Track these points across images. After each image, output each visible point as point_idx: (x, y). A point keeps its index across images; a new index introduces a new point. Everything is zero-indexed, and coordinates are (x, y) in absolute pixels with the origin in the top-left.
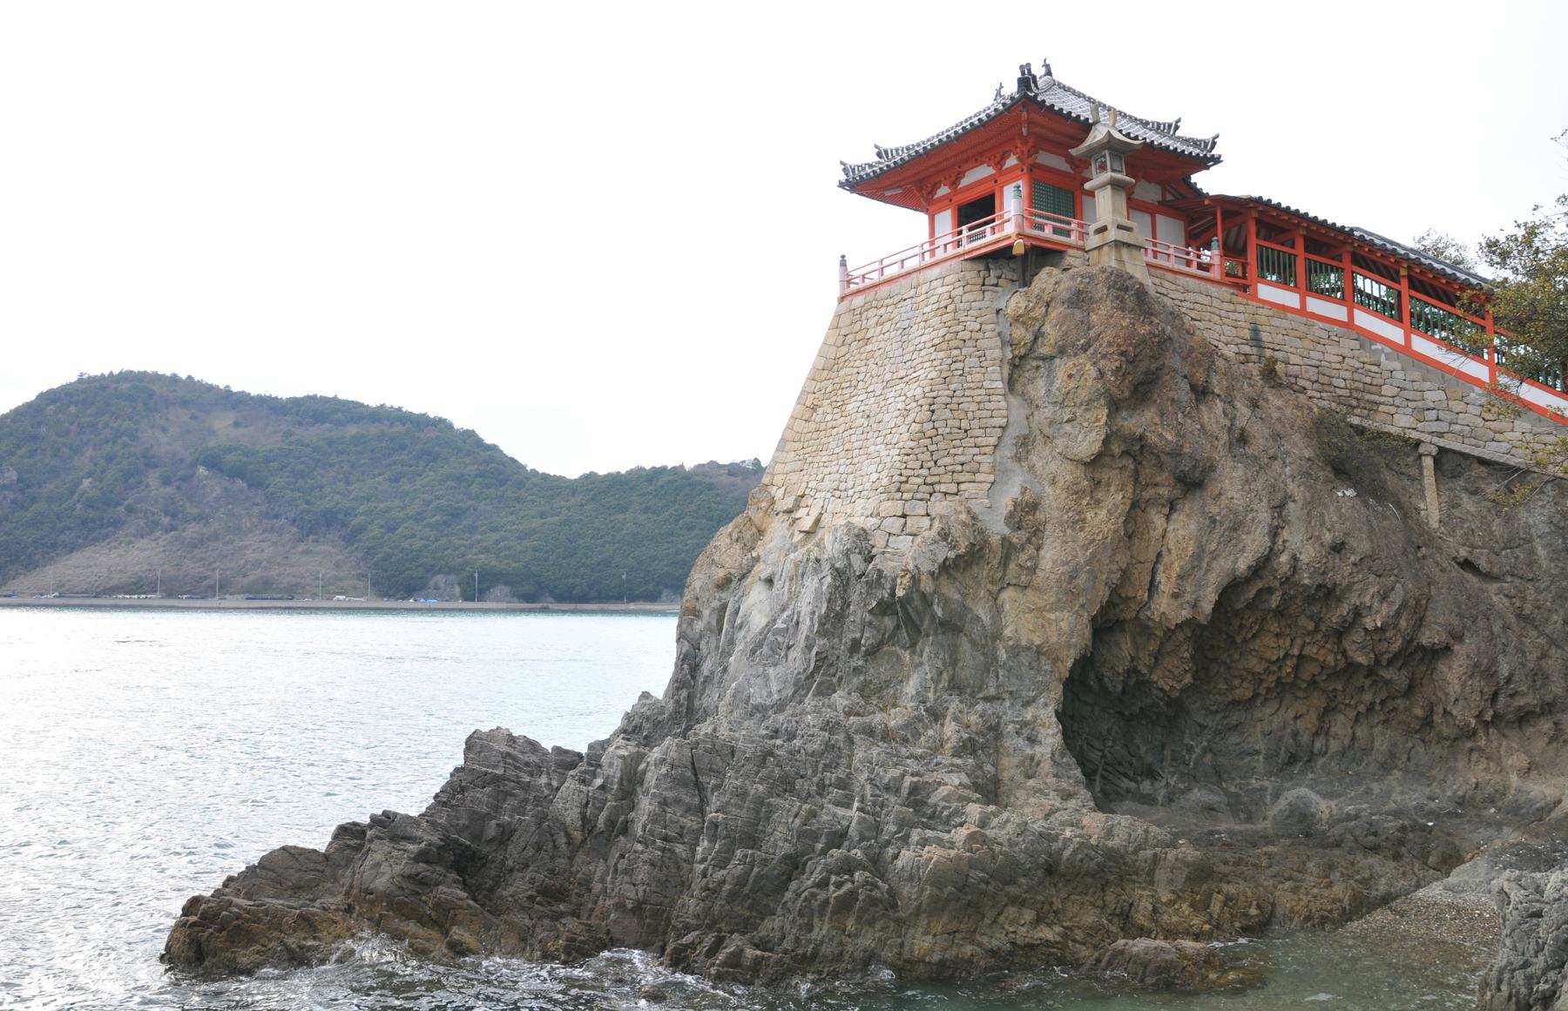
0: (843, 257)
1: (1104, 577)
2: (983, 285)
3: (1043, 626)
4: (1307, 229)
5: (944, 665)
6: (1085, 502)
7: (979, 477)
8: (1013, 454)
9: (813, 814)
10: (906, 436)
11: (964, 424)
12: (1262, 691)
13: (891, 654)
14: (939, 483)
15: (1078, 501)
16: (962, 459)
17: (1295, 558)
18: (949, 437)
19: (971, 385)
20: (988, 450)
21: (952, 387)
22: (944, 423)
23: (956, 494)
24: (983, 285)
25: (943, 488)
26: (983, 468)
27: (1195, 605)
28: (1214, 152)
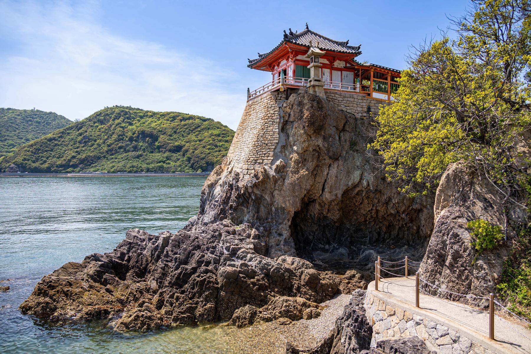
0: (248, 89)
2: (276, 99)
4: (391, 73)
5: (255, 212)
7: (269, 158)
9: (203, 256)
10: (251, 146)
11: (266, 142)
12: (368, 219)
13: (241, 209)
15: (298, 165)
16: (264, 153)
21: (264, 131)
24: (276, 99)
25: (259, 161)
27: (336, 195)
28: (359, 51)
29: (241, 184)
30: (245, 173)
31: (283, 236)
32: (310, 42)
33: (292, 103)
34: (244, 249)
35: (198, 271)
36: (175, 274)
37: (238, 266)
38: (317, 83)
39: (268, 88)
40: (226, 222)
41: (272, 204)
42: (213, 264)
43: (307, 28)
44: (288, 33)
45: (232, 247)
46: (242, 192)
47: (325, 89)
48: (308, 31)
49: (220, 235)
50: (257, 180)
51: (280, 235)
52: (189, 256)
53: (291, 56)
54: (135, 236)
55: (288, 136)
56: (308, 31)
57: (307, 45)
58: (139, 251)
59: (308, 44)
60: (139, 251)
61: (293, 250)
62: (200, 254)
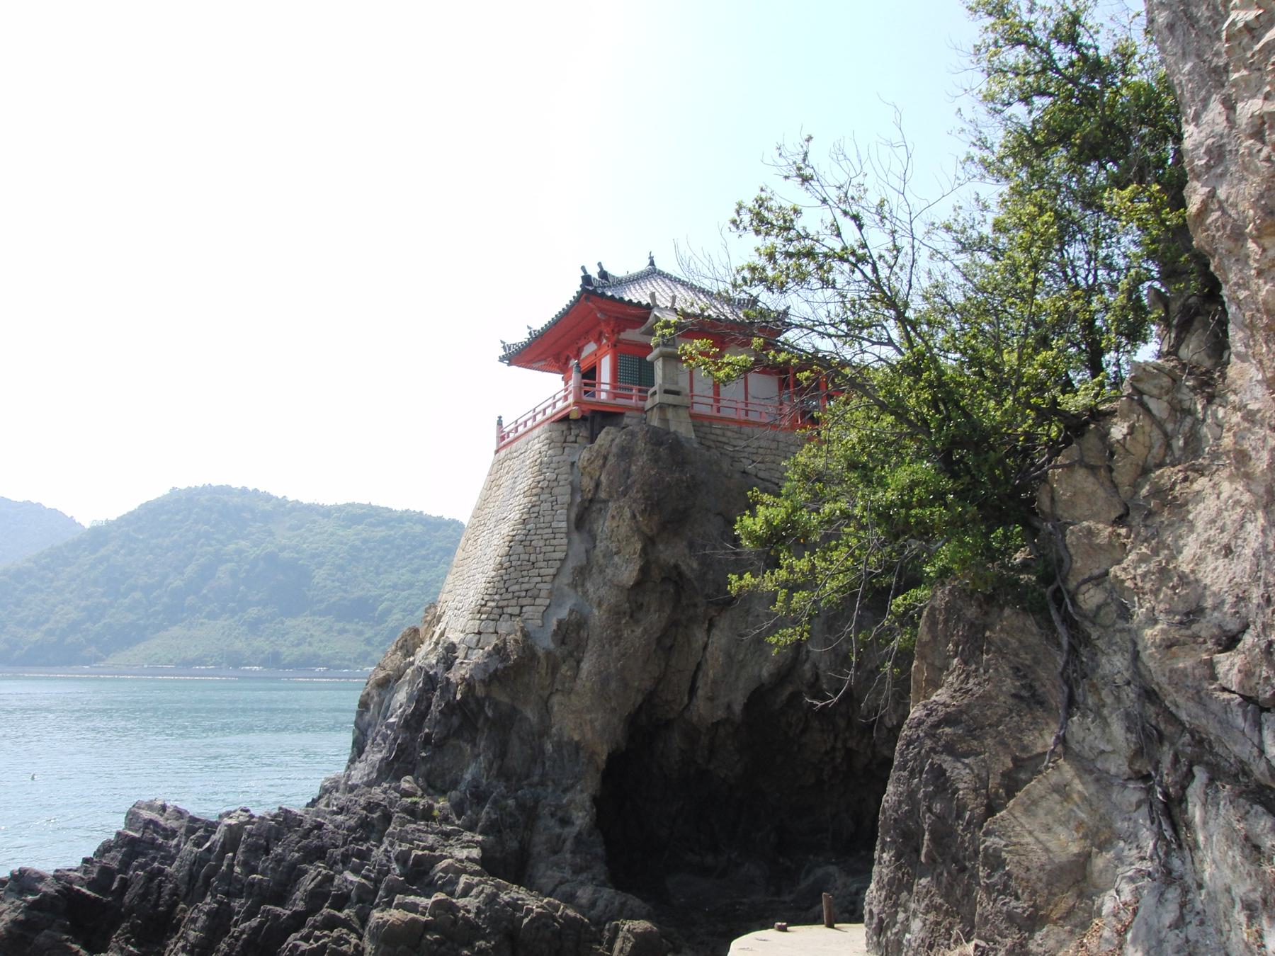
0: (500, 417)
1: (636, 684)
2: (565, 442)
3: (581, 724)
5: (494, 756)
6: (624, 621)
7: (538, 601)
8: (570, 581)
11: (533, 558)
14: (508, 606)
16: (525, 586)
17: (815, 667)
18: (519, 568)
19: (543, 525)
20: (548, 579)
21: (528, 527)
22: (517, 557)
23: (519, 615)
24: (565, 442)
25: (509, 610)
26: (543, 593)
27: (729, 707)
29: (455, 675)
30: (473, 646)
31: (573, 824)
32: (653, 296)
33: (604, 452)
34: (450, 861)
35: (310, 921)
36: (242, 932)
37: (425, 908)
38: (670, 399)
39: (544, 414)
40: (406, 783)
41: (544, 732)
42: (357, 903)
43: (652, 263)
44: (594, 273)
45: (414, 853)
46: (459, 697)
47: (693, 416)
48: (652, 272)
49: (387, 818)
50: (501, 662)
51: (565, 822)
52: (293, 874)
53: (606, 330)
54: (151, 821)
55: (593, 537)
56: (652, 272)
57: (644, 303)
58: (156, 864)
59: (645, 300)
60: (156, 864)
61: (600, 869)
62: (319, 873)
